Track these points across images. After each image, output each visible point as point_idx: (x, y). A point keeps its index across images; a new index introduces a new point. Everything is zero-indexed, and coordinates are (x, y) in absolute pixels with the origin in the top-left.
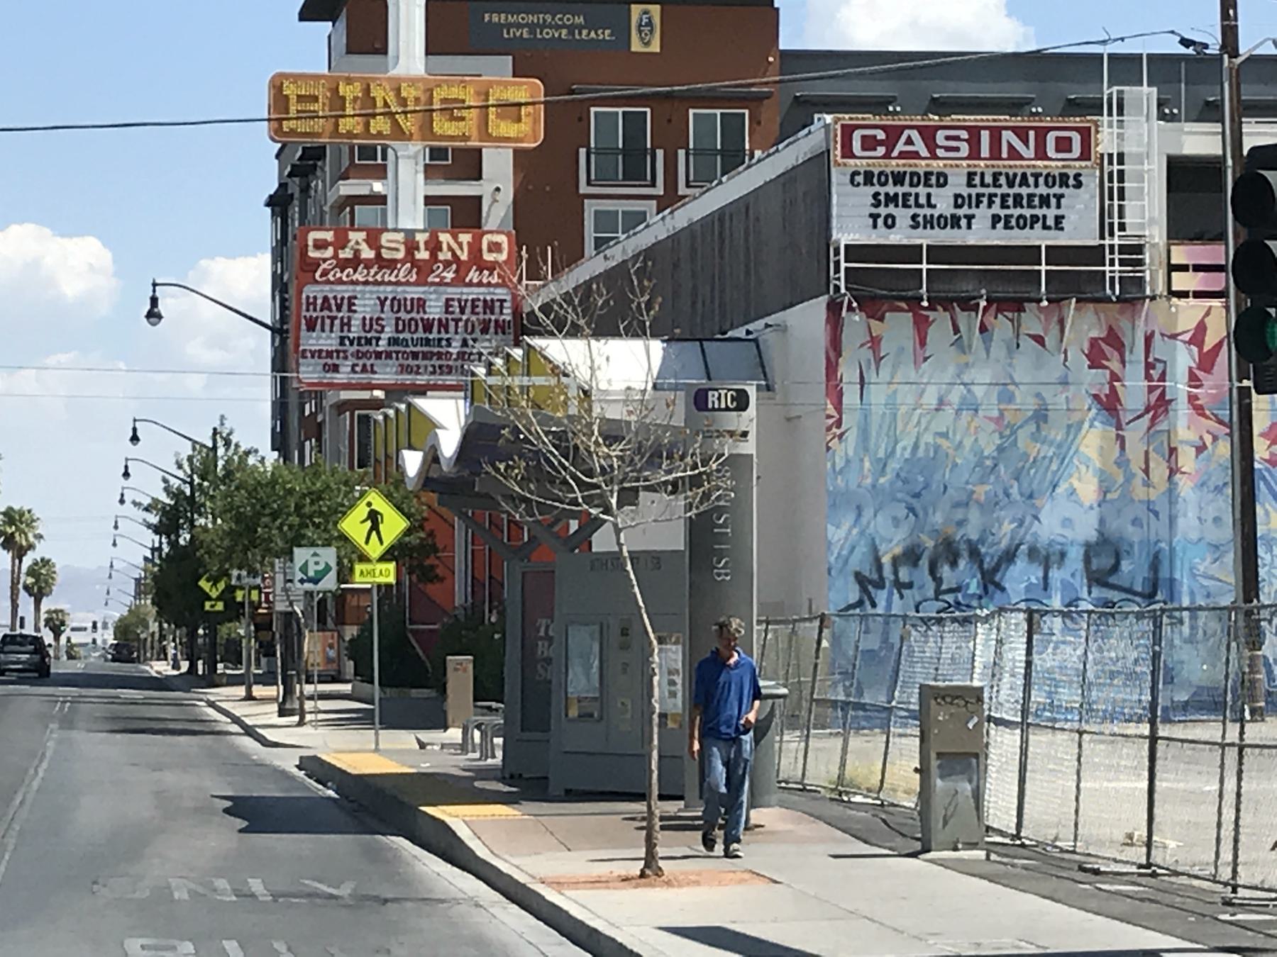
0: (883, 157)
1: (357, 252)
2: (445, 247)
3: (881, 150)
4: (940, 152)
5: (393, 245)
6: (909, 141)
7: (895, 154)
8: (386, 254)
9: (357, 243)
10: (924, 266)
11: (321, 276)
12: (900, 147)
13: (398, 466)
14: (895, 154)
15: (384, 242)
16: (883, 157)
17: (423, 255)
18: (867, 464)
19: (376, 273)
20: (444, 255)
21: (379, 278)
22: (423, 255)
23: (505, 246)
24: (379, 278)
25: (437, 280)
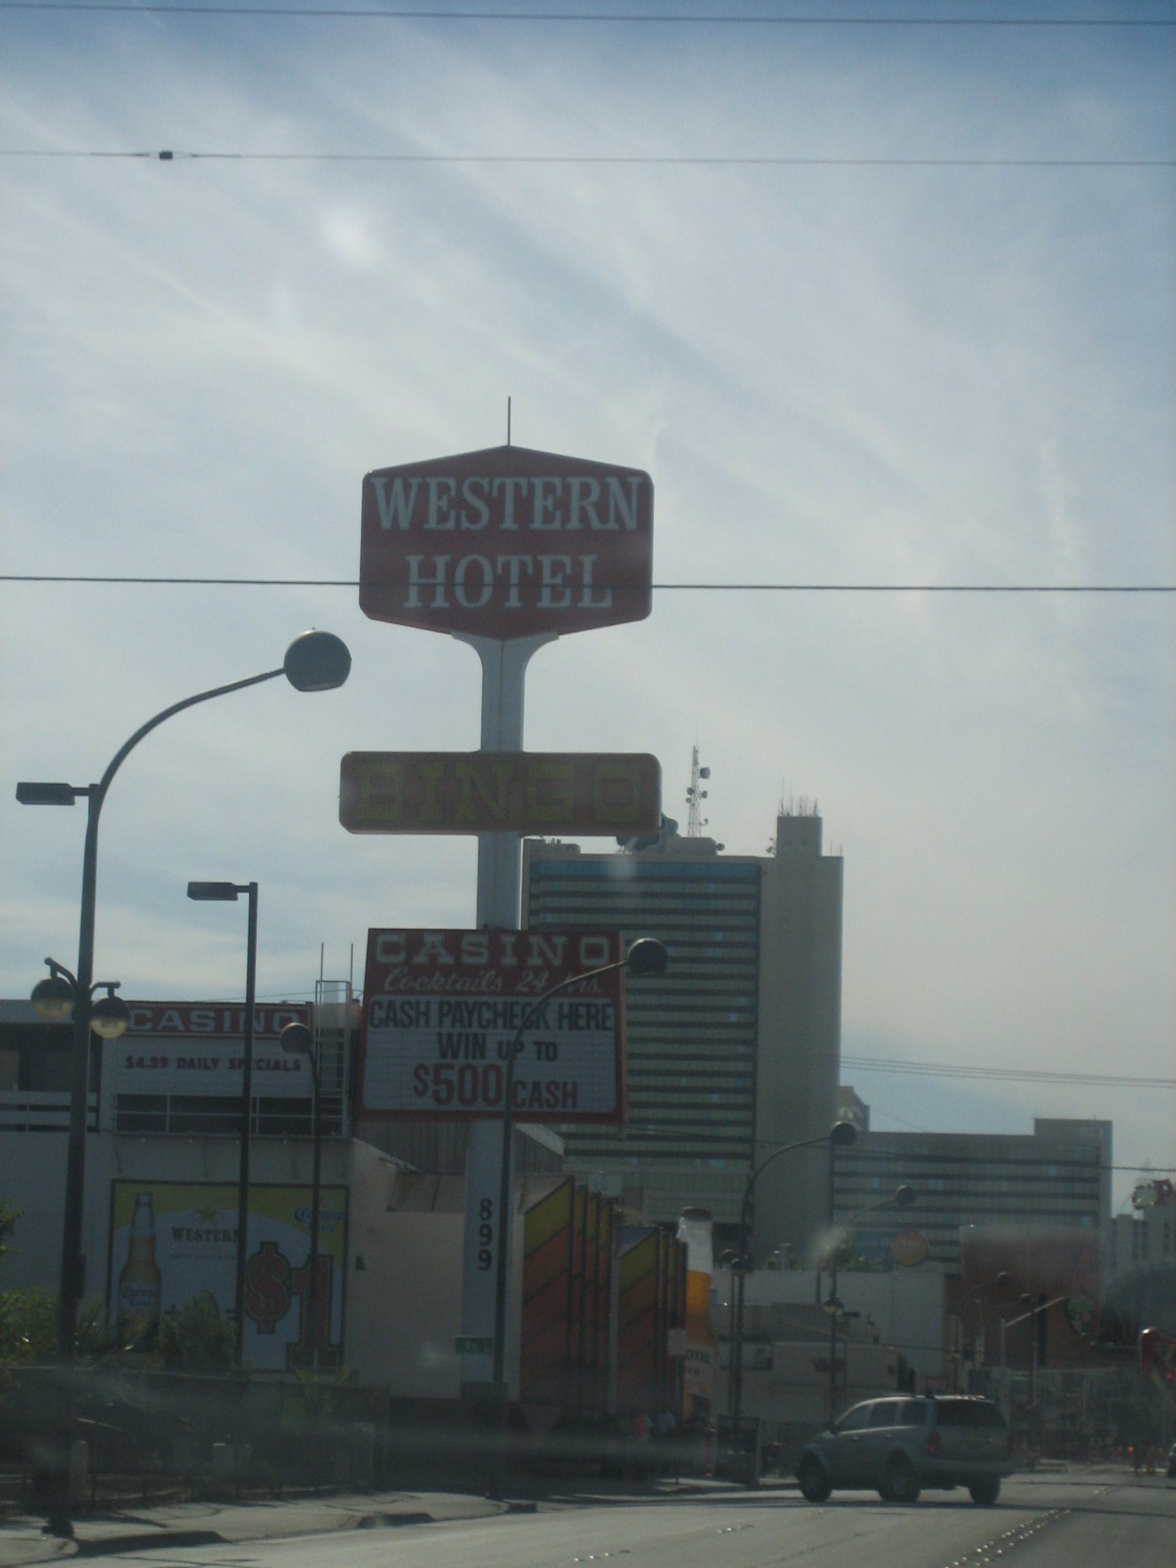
0: (151, 1030)
1: (433, 958)
2: (535, 950)
3: (149, 1026)
4: (193, 1027)
5: (474, 949)
6: (170, 1019)
7: (160, 1028)
8: (467, 960)
9: (433, 947)
10: (168, 1113)
11: (391, 985)
12: (164, 1022)
13: (667, 1469)
14: (160, 1028)
15: (465, 946)
16: (151, 1030)
17: (509, 960)
18: (626, 1247)
19: (455, 982)
20: (535, 961)
21: (458, 986)
22: (509, 960)
23: (582, 953)
24: (458, 986)
25: (526, 990)
